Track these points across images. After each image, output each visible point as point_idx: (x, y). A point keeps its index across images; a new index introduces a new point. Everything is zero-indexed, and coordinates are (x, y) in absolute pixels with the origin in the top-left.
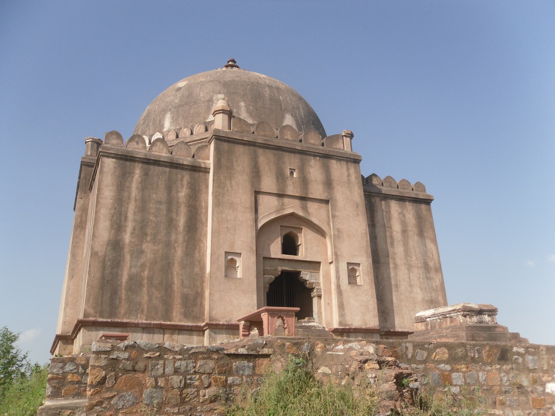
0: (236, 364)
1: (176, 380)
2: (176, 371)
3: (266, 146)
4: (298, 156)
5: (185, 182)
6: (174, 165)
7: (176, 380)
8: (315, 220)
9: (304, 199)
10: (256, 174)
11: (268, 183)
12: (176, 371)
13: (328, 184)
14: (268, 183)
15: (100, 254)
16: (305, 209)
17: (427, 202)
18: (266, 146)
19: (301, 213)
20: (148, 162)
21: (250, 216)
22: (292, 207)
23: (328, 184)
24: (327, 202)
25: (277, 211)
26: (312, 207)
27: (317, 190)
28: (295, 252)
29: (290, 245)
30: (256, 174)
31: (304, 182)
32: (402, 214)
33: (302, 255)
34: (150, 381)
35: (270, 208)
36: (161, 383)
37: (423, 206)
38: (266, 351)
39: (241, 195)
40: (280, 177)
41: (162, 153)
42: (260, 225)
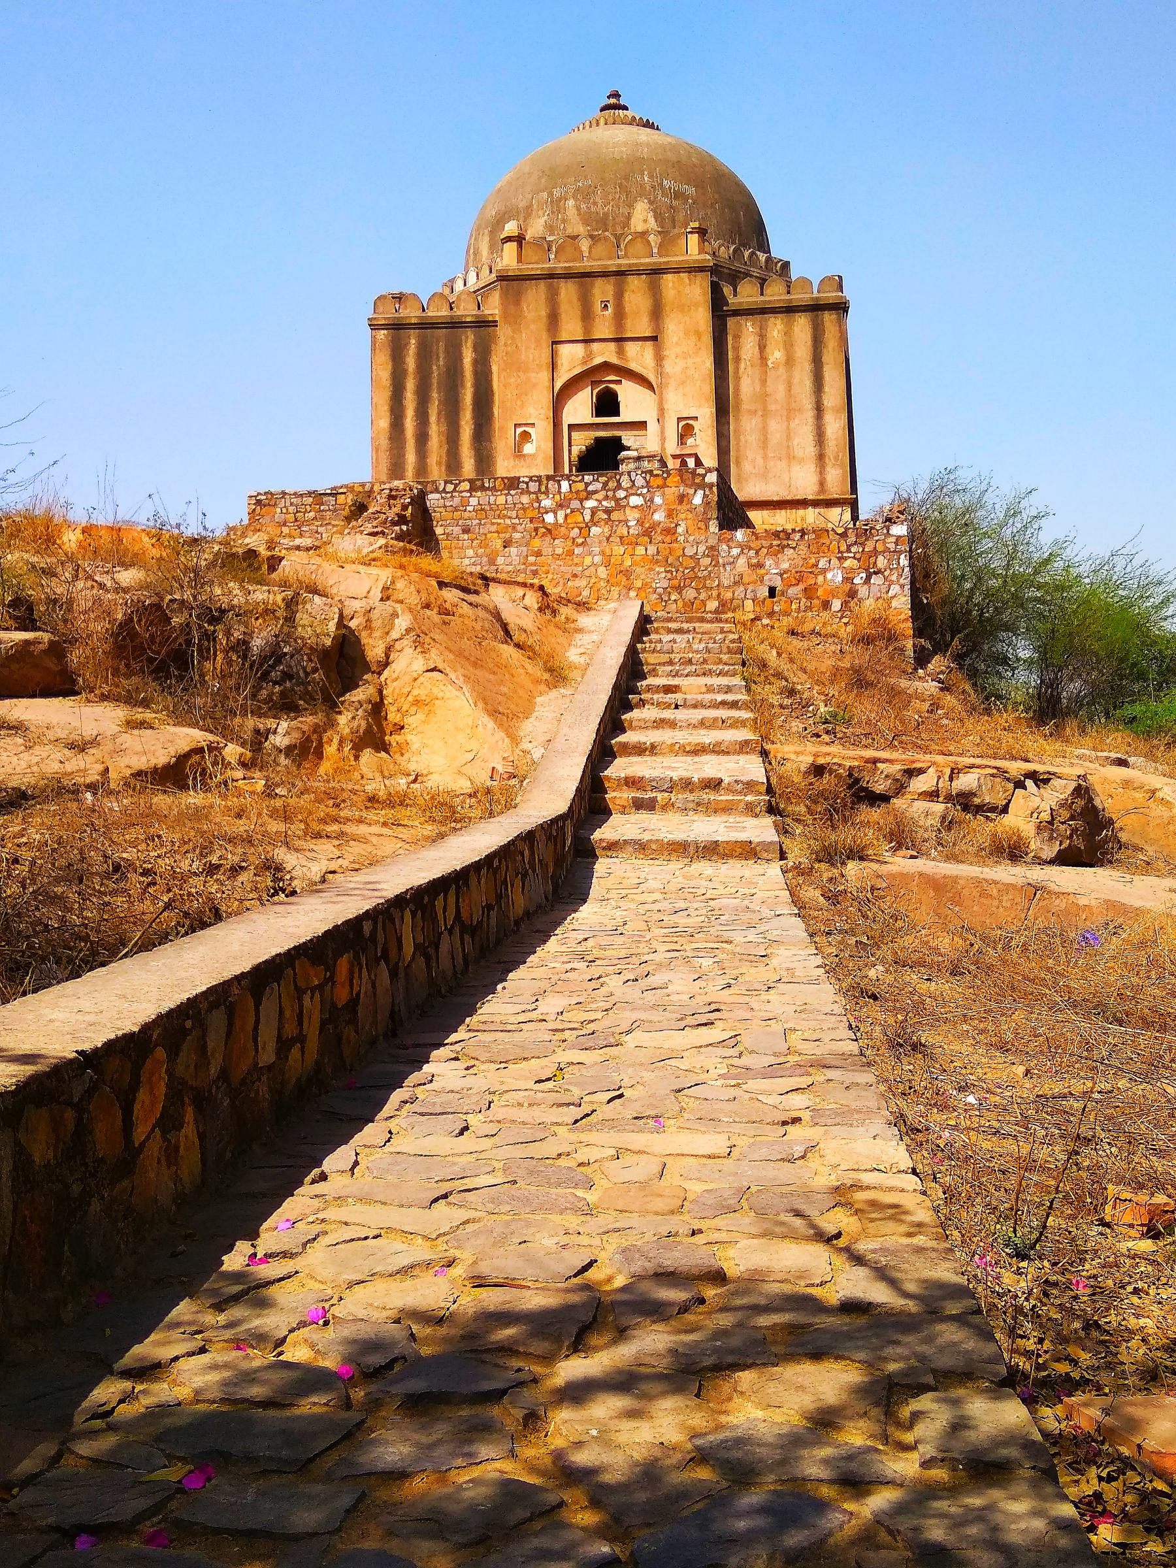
0: (325, 499)
1: (291, 509)
2: (292, 504)
3: (568, 276)
4: (612, 279)
5: (470, 343)
6: (455, 325)
7: (291, 509)
8: (633, 366)
9: (619, 340)
10: (554, 320)
11: (571, 326)
12: (292, 504)
13: (657, 313)
14: (571, 326)
15: (971, 1435)
16: (621, 352)
17: (841, 308)
18: (568, 276)
19: (614, 360)
20: (426, 325)
21: (545, 375)
22: (605, 353)
23: (657, 313)
24: (654, 338)
25: (585, 363)
26: (632, 348)
27: (640, 325)
28: (617, 413)
29: (607, 404)
30: (554, 320)
31: (620, 316)
32: (788, 333)
33: (626, 415)
34: (278, 510)
35: (572, 358)
36: (284, 510)
37: (829, 318)
38: (341, 491)
39: (535, 353)
40: (587, 316)
41: (440, 312)
42: (559, 384)
